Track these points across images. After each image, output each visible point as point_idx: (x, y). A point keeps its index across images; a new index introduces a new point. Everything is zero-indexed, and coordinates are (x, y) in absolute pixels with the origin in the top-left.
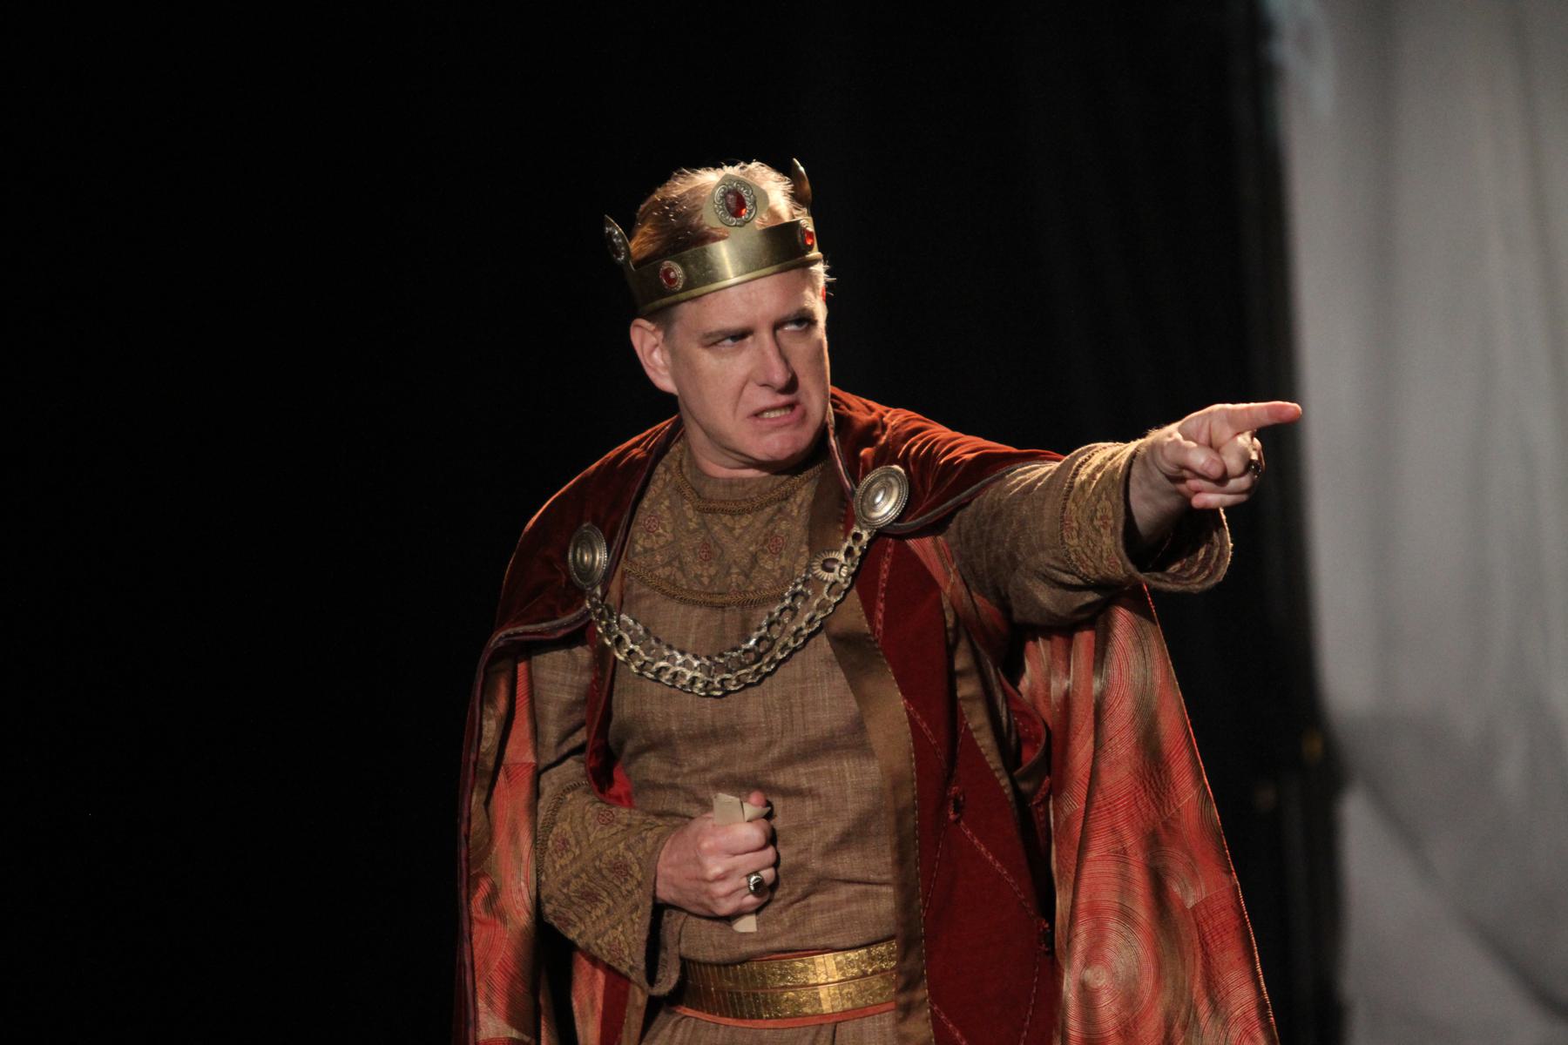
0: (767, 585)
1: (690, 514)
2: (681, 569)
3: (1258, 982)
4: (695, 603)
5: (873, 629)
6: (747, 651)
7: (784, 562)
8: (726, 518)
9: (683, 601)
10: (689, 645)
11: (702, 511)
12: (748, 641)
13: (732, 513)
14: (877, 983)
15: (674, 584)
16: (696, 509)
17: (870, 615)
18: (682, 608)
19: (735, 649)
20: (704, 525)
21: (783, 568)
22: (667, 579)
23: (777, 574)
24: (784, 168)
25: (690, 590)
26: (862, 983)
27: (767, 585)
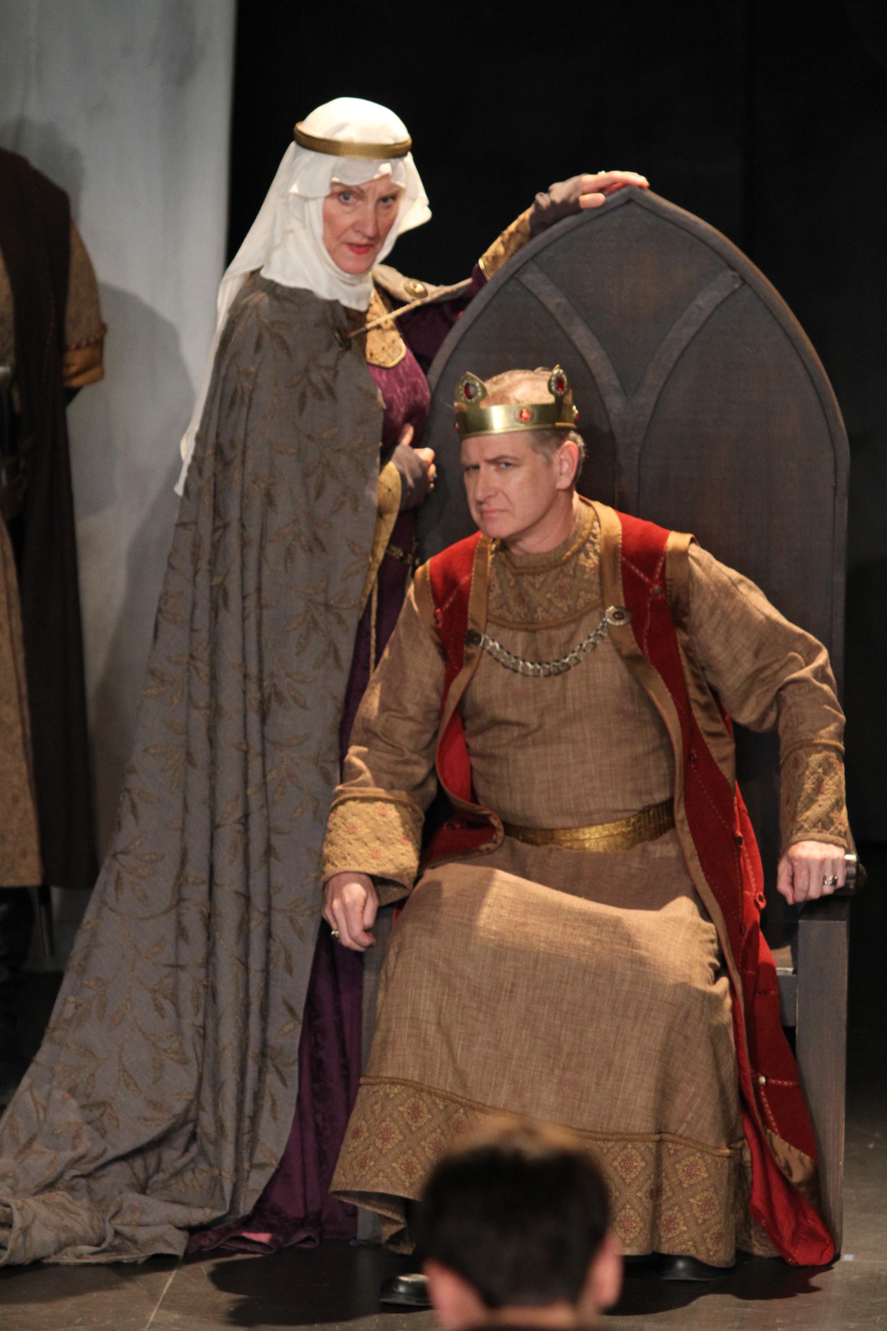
0: (560, 616)
1: (510, 576)
2: (509, 610)
3: (247, 1014)
4: (518, 629)
5: (644, 653)
6: (563, 664)
7: (570, 602)
8: (530, 578)
9: (511, 629)
10: (519, 654)
11: (515, 575)
12: (565, 658)
13: (533, 575)
14: (619, 840)
15: (505, 619)
16: (513, 574)
17: (641, 645)
18: (511, 633)
19: (557, 661)
20: (517, 583)
21: (569, 606)
22: (500, 617)
23: (566, 609)
24: (479, 267)
25: (514, 622)
26: (611, 839)
27: (560, 616)
